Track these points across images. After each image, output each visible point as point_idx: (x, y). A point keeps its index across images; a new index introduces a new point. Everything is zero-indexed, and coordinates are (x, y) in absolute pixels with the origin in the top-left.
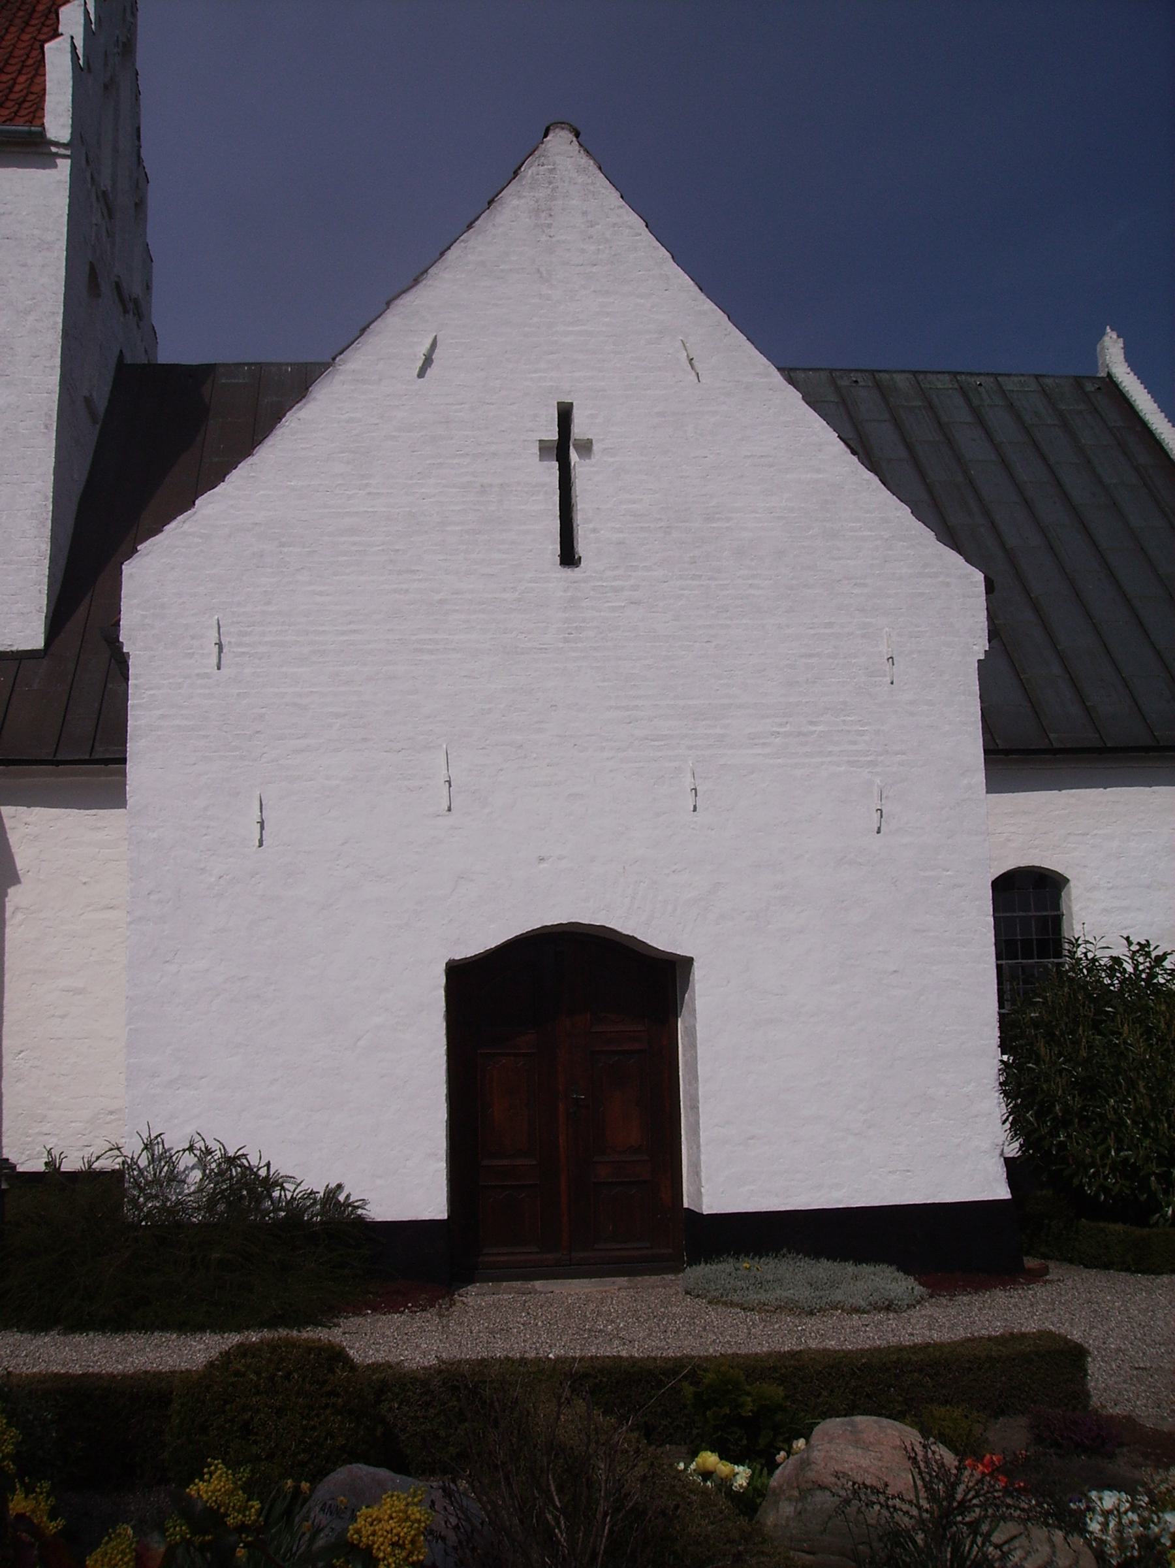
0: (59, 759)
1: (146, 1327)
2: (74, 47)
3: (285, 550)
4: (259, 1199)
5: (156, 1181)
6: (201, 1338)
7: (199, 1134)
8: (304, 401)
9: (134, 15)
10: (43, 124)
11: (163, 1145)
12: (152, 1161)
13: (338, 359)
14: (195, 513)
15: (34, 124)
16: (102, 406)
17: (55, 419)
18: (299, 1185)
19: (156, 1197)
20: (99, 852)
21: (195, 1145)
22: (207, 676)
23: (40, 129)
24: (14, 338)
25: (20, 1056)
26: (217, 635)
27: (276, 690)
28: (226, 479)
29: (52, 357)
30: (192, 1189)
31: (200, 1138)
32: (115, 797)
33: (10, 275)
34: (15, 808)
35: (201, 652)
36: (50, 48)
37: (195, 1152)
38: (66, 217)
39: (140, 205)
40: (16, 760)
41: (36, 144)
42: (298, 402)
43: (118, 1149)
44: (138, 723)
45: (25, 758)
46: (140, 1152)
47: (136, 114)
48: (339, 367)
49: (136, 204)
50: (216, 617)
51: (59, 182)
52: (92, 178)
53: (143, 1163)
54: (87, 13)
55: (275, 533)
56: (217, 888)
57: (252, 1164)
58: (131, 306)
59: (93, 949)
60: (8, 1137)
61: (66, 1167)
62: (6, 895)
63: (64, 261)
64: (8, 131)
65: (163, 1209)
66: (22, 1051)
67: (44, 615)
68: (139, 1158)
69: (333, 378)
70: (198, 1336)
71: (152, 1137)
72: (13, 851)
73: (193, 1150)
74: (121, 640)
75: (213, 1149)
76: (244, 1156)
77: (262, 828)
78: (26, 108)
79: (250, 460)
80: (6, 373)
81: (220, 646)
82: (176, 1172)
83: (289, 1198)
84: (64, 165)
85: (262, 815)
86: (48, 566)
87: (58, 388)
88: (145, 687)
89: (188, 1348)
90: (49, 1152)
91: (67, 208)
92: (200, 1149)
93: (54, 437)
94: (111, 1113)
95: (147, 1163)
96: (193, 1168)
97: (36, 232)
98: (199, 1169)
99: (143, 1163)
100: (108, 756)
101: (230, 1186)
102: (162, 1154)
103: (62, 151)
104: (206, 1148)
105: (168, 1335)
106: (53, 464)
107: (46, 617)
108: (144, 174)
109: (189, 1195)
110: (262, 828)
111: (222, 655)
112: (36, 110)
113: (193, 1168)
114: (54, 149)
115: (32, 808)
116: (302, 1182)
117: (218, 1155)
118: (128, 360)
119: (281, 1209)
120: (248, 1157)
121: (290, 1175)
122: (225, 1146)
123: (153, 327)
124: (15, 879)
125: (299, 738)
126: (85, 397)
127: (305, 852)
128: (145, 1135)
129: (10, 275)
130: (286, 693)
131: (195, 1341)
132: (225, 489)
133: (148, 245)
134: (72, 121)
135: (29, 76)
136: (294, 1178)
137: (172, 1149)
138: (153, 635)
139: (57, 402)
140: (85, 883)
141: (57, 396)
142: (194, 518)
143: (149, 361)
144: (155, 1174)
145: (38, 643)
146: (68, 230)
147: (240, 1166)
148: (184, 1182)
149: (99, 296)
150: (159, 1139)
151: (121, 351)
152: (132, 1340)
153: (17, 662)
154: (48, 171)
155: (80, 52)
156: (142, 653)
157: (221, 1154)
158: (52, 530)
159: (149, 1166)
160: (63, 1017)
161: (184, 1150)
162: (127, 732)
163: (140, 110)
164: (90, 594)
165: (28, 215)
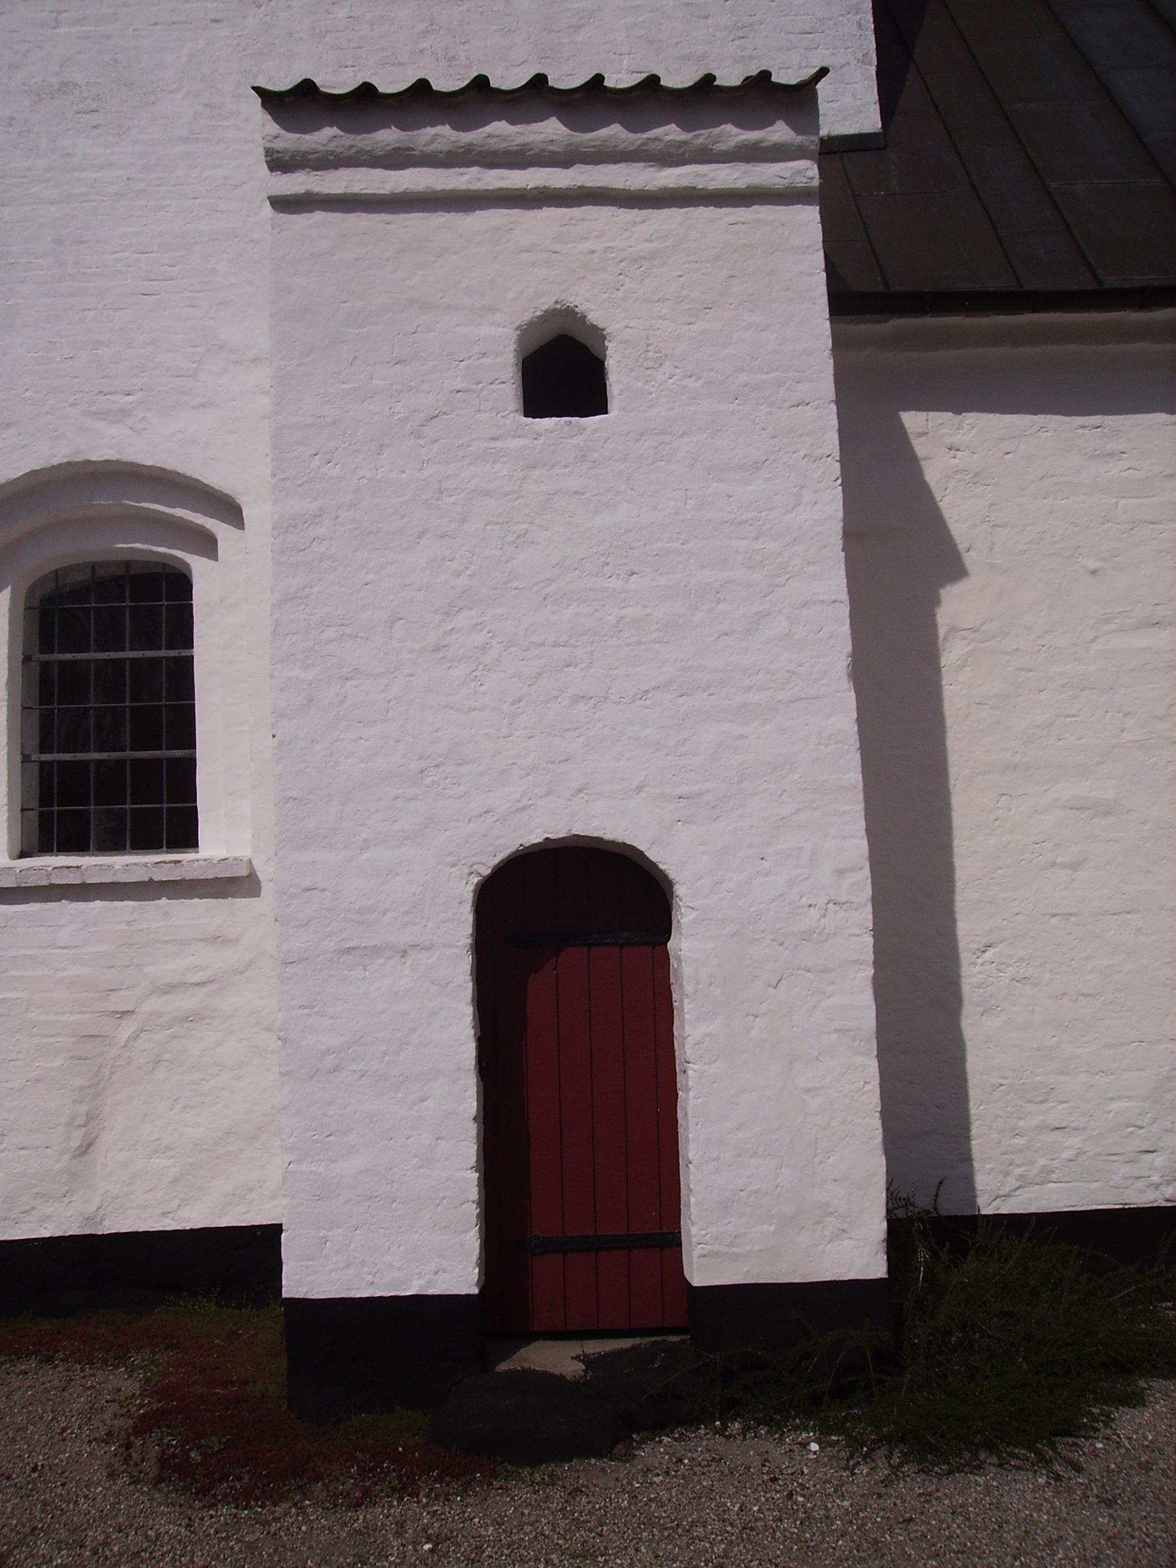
25: (988, 955)
160: (1075, 866)
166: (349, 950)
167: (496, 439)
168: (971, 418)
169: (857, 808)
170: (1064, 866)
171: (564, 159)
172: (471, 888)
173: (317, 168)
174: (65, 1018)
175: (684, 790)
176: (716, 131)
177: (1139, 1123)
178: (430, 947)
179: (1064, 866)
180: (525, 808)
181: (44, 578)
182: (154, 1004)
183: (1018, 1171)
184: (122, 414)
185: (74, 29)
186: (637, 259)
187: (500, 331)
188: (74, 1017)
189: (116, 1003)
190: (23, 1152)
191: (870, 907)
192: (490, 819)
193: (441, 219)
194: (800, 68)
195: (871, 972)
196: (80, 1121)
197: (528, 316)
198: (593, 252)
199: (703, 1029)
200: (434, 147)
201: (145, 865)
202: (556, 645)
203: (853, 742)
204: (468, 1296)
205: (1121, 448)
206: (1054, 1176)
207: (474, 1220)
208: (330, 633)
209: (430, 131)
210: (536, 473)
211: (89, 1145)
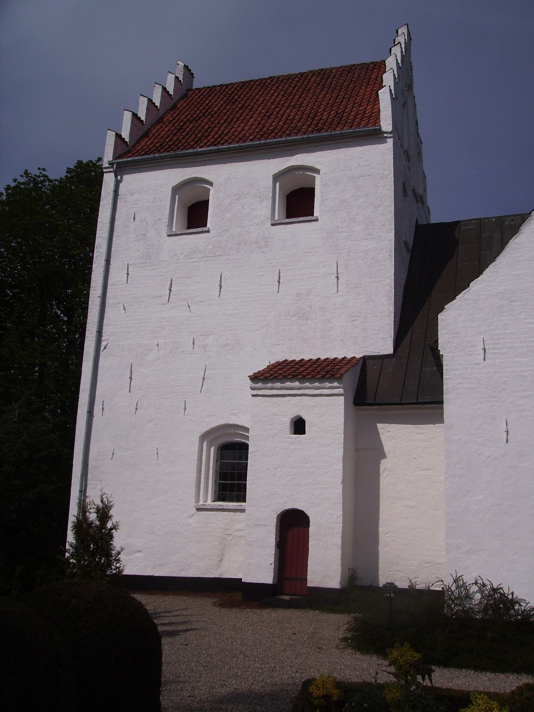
0: (403, 402)
1: (460, 666)
2: (391, 90)
3: (513, 304)
4: (507, 609)
5: (459, 598)
6: (486, 674)
7: (480, 577)
8: (518, 234)
9: (411, 72)
10: (380, 125)
11: (463, 581)
12: (458, 587)
13: (532, 213)
14: (470, 290)
15: (376, 125)
16: (411, 244)
17: (394, 252)
18: (527, 604)
19: (460, 605)
20: (421, 444)
21: (478, 582)
22: (479, 364)
23: (379, 127)
24: (374, 218)
25: (387, 535)
26: (483, 345)
27: (512, 369)
28: (483, 273)
29: (390, 225)
30: (477, 602)
31: (480, 579)
32: (438, 418)
33: (370, 191)
34: (383, 424)
35: (476, 353)
36: (381, 93)
37: (478, 585)
38: (393, 163)
39: (419, 154)
40: (383, 403)
41: (378, 134)
42: (514, 235)
43: (442, 581)
44: (449, 386)
45: (388, 402)
46: (452, 583)
47: (415, 114)
48: (533, 217)
49: (418, 154)
50: (482, 337)
51: (388, 148)
52: (401, 145)
53: (453, 588)
54: (394, 75)
55: (508, 296)
56: (487, 462)
57: (505, 592)
58: (419, 199)
59: (419, 488)
60: (381, 571)
61: (417, 587)
62: (380, 463)
63: (393, 183)
64: (367, 130)
65: (463, 611)
66: (388, 533)
67: (392, 339)
68: (451, 586)
69: (531, 222)
70: (484, 673)
71: (458, 577)
72: (383, 443)
73: (477, 584)
74: (439, 349)
75: (486, 584)
76: (501, 588)
77: (508, 434)
78: (372, 120)
79: (494, 263)
80: (371, 234)
81: (484, 350)
82: (469, 594)
83: (523, 610)
84: (390, 141)
85: (507, 428)
86: (393, 317)
87: (394, 238)
88: (451, 370)
89: (480, 679)
90: (410, 581)
91: (393, 159)
92: (481, 584)
93: (393, 260)
94: (427, 563)
95: (455, 589)
96: (477, 592)
97: (380, 171)
98: (479, 593)
99: (453, 588)
100: (424, 401)
101: (495, 602)
102: (462, 585)
103: (389, 135)
104: (483, 583)
105: (469, 671)
106: (393, 272)
107: (393, 339)
108: (420, 141)
109: (475, 605)
110: (508, 434)
111: (486, 354)
112: (376, 120)
113: (477, 592)
114: (385, 135)
115: (391, 425)
116: (529, 602)
117: (488, 587)
118: (420, 223)
119: (518, 615)
120: (503, 589)
121: (523, 599)
122: (492, 582)
123: (428, 207)
124: (384, 456)
125: (523, 392)
126: (404, 241)
127: (528, 445)
128: (454, 576)
129: (370, 191)
130: (516, 370)
131: (483, 676)
132: (483, 277)
133: (424, 171)
134: (392, 122)
135: (372, 105)
136: (525, 600)
137: (467, 582)
138: (454, 346)
139: (394, 245)
140: (415, 458)
141: (394, 241)
142: (470, 292)
143: (427, 222)
144: (459, 594)
145: (391, 351)
146: (394, 169)
147: (499, 593)
148: (472, 598)
149: (407, 196)
150: (461, 578)
151: (417, 219)
152: (453, 671)
153: (382, 360)
154: (383, 145)
155: (393, 92)
156: (449, 354)
157: (491, 587)
158: (394, 301)
159: (456, 590)
160: (406, 518)
161: (473, 584)
162: (443, 391)
163: (416, 112)
164: (411, 329)
165: (376, 164)
166: (256, 525)
167: (286, 439)
168: (393, 425)
169: (341, 506)
170: (404, 518)
171: (300, 389)
172: (276, 516)
173: (258, 390)
174: (219, 535)
175: (312, 501)
176: (325, 384)
177: (415, 571)
178: (269, 525)
179: (404, 518)
180: (286, 503)
181: (221, 445)
182: (235, 533)
183: (390, 579)
184: (235, 414)
185: (230, 332)
186: (312, 406)
187: (287, 419)
188: (220, 535)
189: (229, 533)
190: (209, 560)
191: (342, 524)
192: (280, 504)
193: (279, 398)
194: (377, 339)
195: (341, 535)
196: (220, 555)
197: (292, 417)
198: (304, 405)
199: (312, 542)
200: (277, 387)
201: (235, 506)
202: (293, 475)
203: (341, 495)
204: (271, 584)
205: (423, 432)
206: (397, 580)
207: (273, 571)
208: (257, 471)
209: (277, 384)
210: (292, 445)
211: (221, 560)
